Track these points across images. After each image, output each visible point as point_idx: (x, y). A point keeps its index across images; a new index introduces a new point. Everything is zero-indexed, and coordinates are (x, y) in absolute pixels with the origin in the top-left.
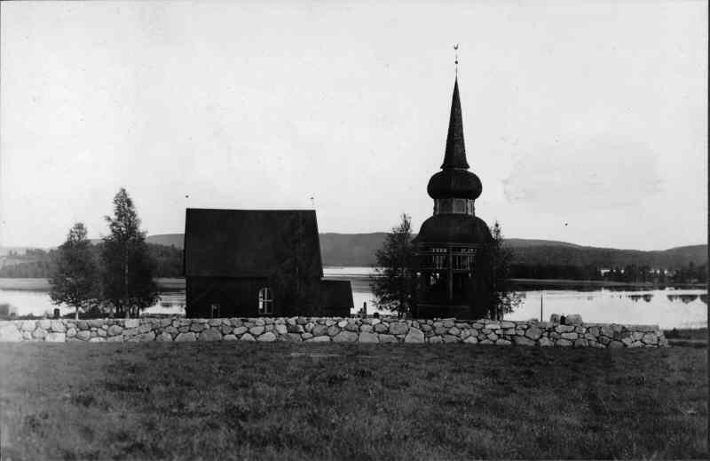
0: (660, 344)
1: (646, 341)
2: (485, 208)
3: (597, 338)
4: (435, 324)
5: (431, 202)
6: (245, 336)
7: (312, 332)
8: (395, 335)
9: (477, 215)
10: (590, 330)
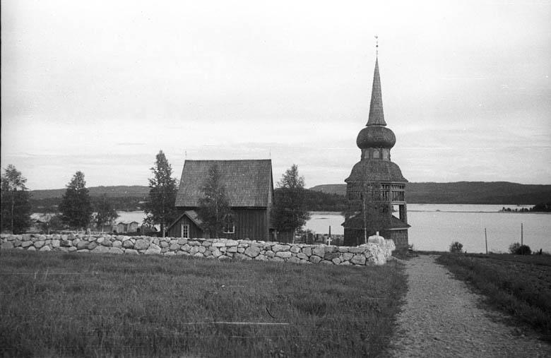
0: (368, 264)
1: (354, 261)
2: (395, 155)
3: (309, 257)
4: (171, 242)
5: (359, 151)
6: (30, 248)
7: (77, 246)
8: (138, 250)
9: (392, 161)
10: (304, 249)
